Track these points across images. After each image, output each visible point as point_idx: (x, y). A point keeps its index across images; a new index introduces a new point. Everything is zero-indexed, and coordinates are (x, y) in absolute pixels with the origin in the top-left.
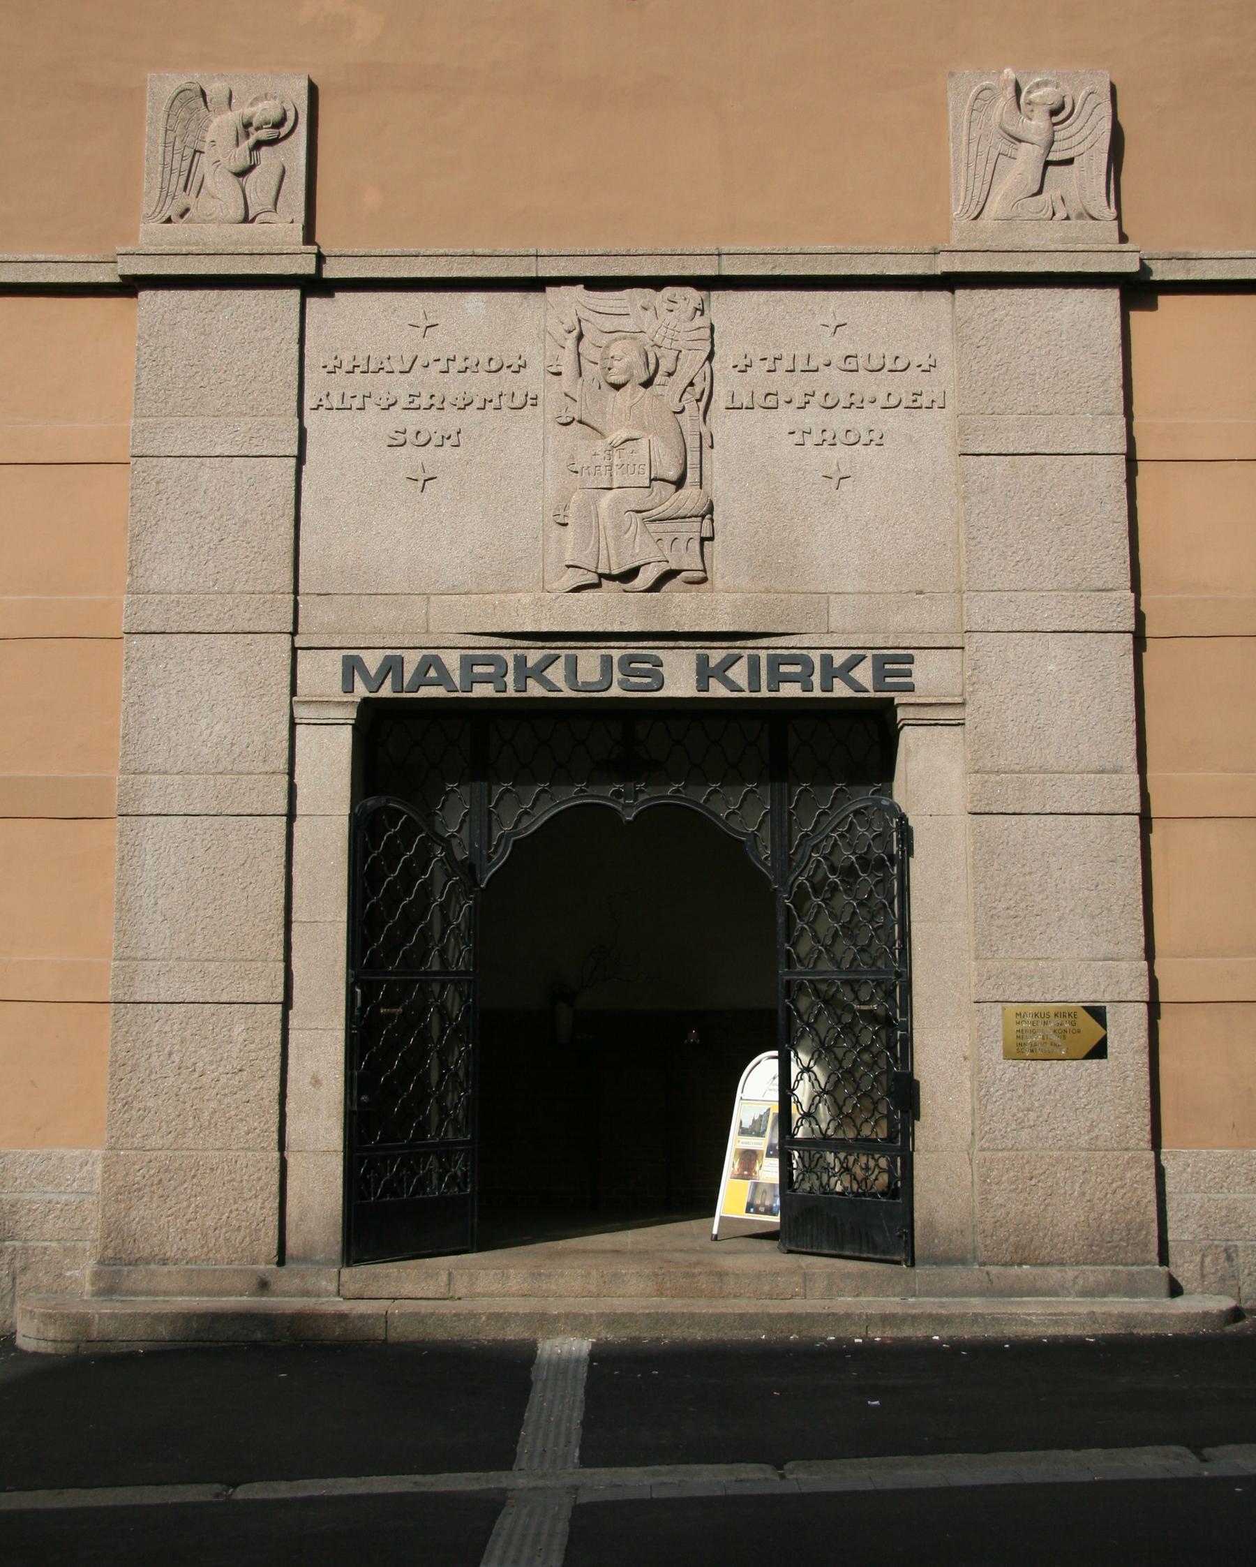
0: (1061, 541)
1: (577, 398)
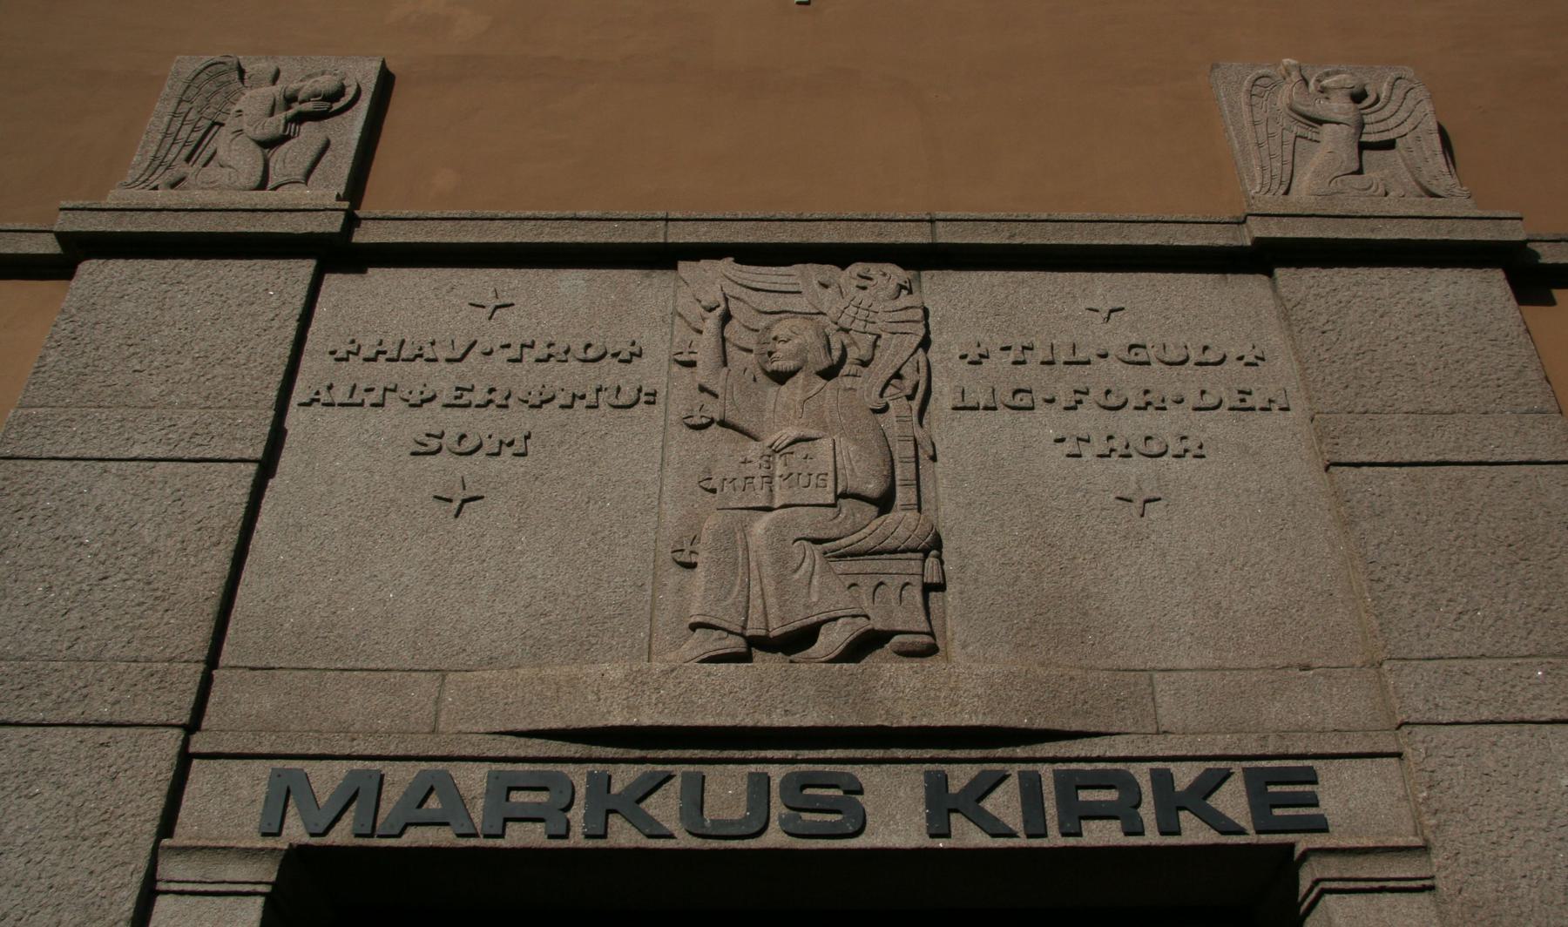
0: (1522, 582)
1: (718, 390)
